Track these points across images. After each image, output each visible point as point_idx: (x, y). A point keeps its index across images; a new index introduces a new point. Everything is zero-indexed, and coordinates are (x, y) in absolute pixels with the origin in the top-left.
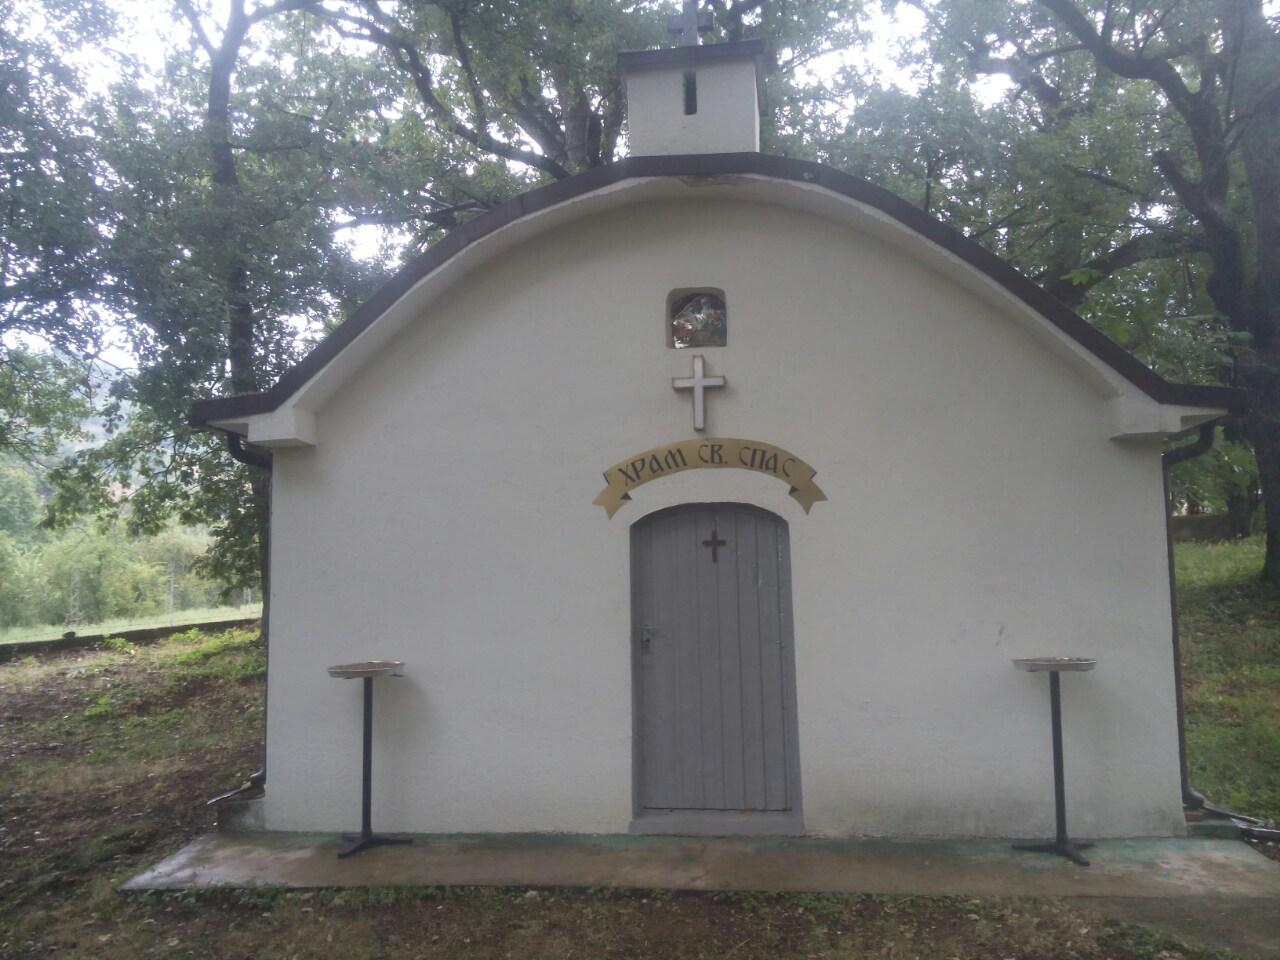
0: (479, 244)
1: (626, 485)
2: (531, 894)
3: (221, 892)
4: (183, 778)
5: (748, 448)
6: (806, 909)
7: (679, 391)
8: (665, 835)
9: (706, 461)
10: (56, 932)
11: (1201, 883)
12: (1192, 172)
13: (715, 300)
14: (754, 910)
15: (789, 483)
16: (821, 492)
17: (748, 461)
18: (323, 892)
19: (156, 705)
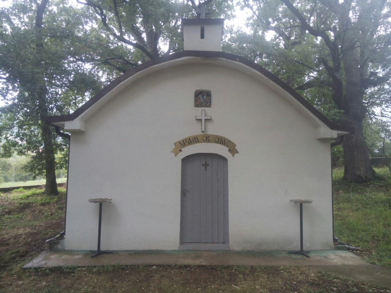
0: (140, 73)
1: (181, 147)
2: (154, 267)
3: (57, 268)
4: (31, 234)
5: (217, 138)
6: (235, 270)
7: (197, 120)
8: (189, 250)
9: (205, 141)
10: (3, 281)
11: (340, 262)
12: (331, 64)
13: (208, 94)
14: (220, 271)
15: (228, 148)
16: (238, 152)
18: (90, 267)
19: (13, 212)
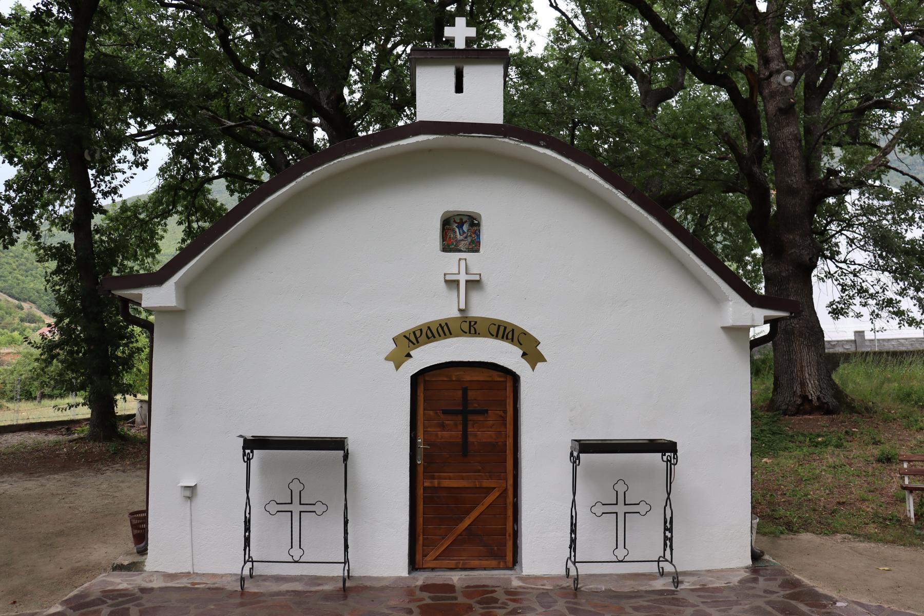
17: (495, 333)
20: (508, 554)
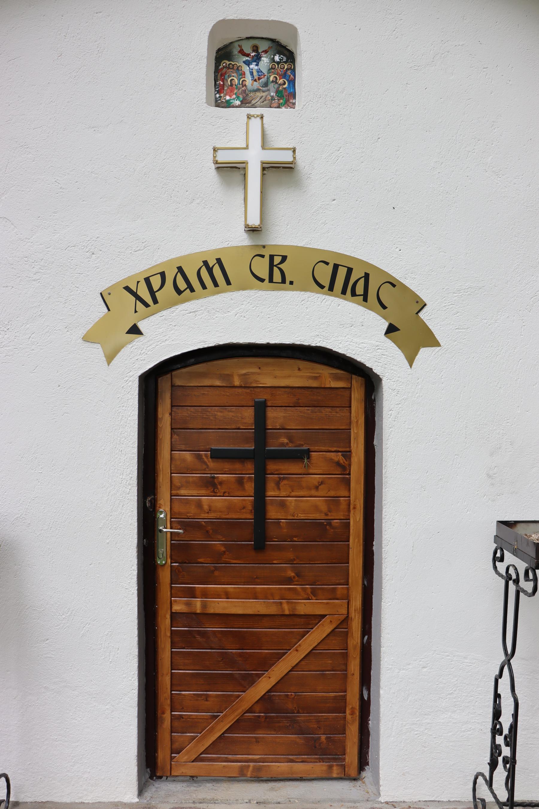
13: (290, 282)
15: (384, 318)
17: (326, 283)
20: (348, 750)
